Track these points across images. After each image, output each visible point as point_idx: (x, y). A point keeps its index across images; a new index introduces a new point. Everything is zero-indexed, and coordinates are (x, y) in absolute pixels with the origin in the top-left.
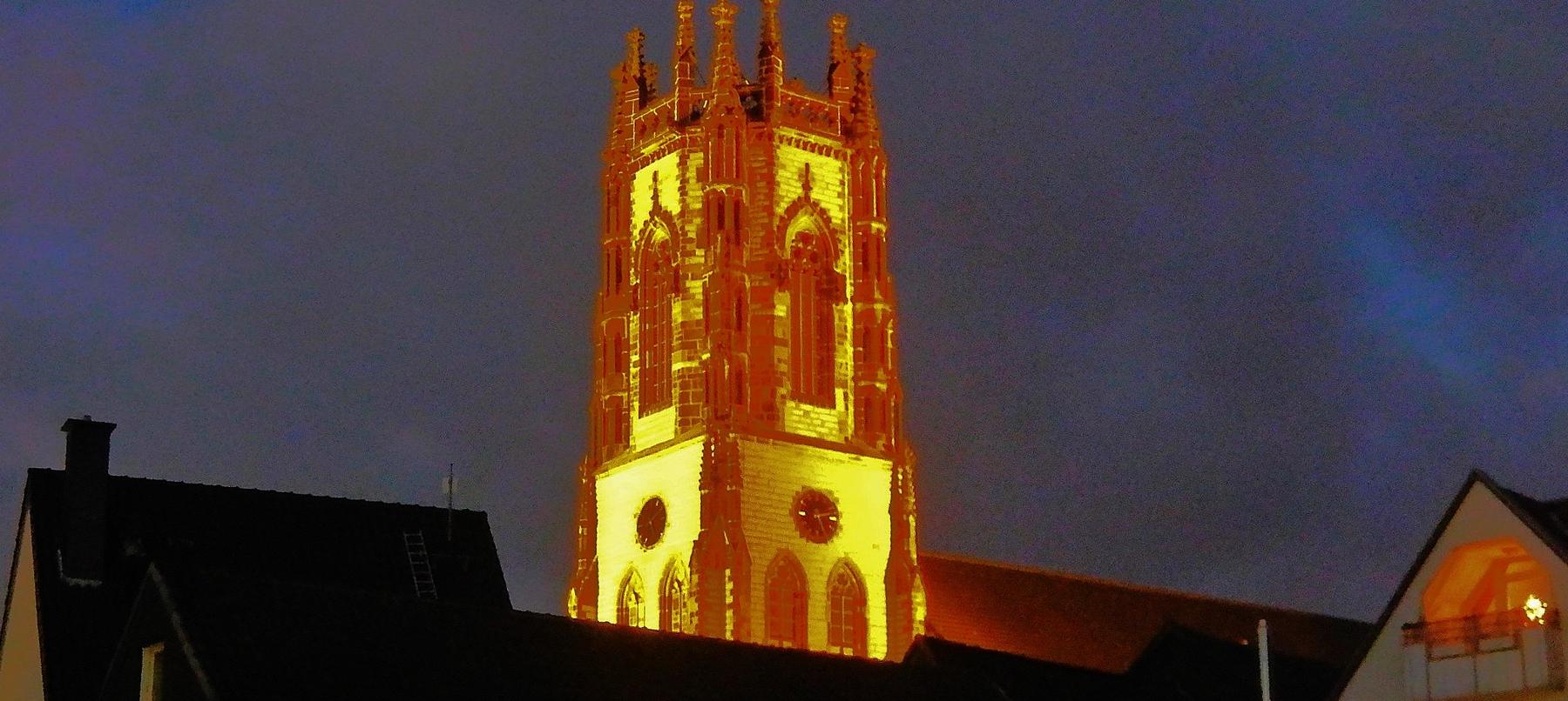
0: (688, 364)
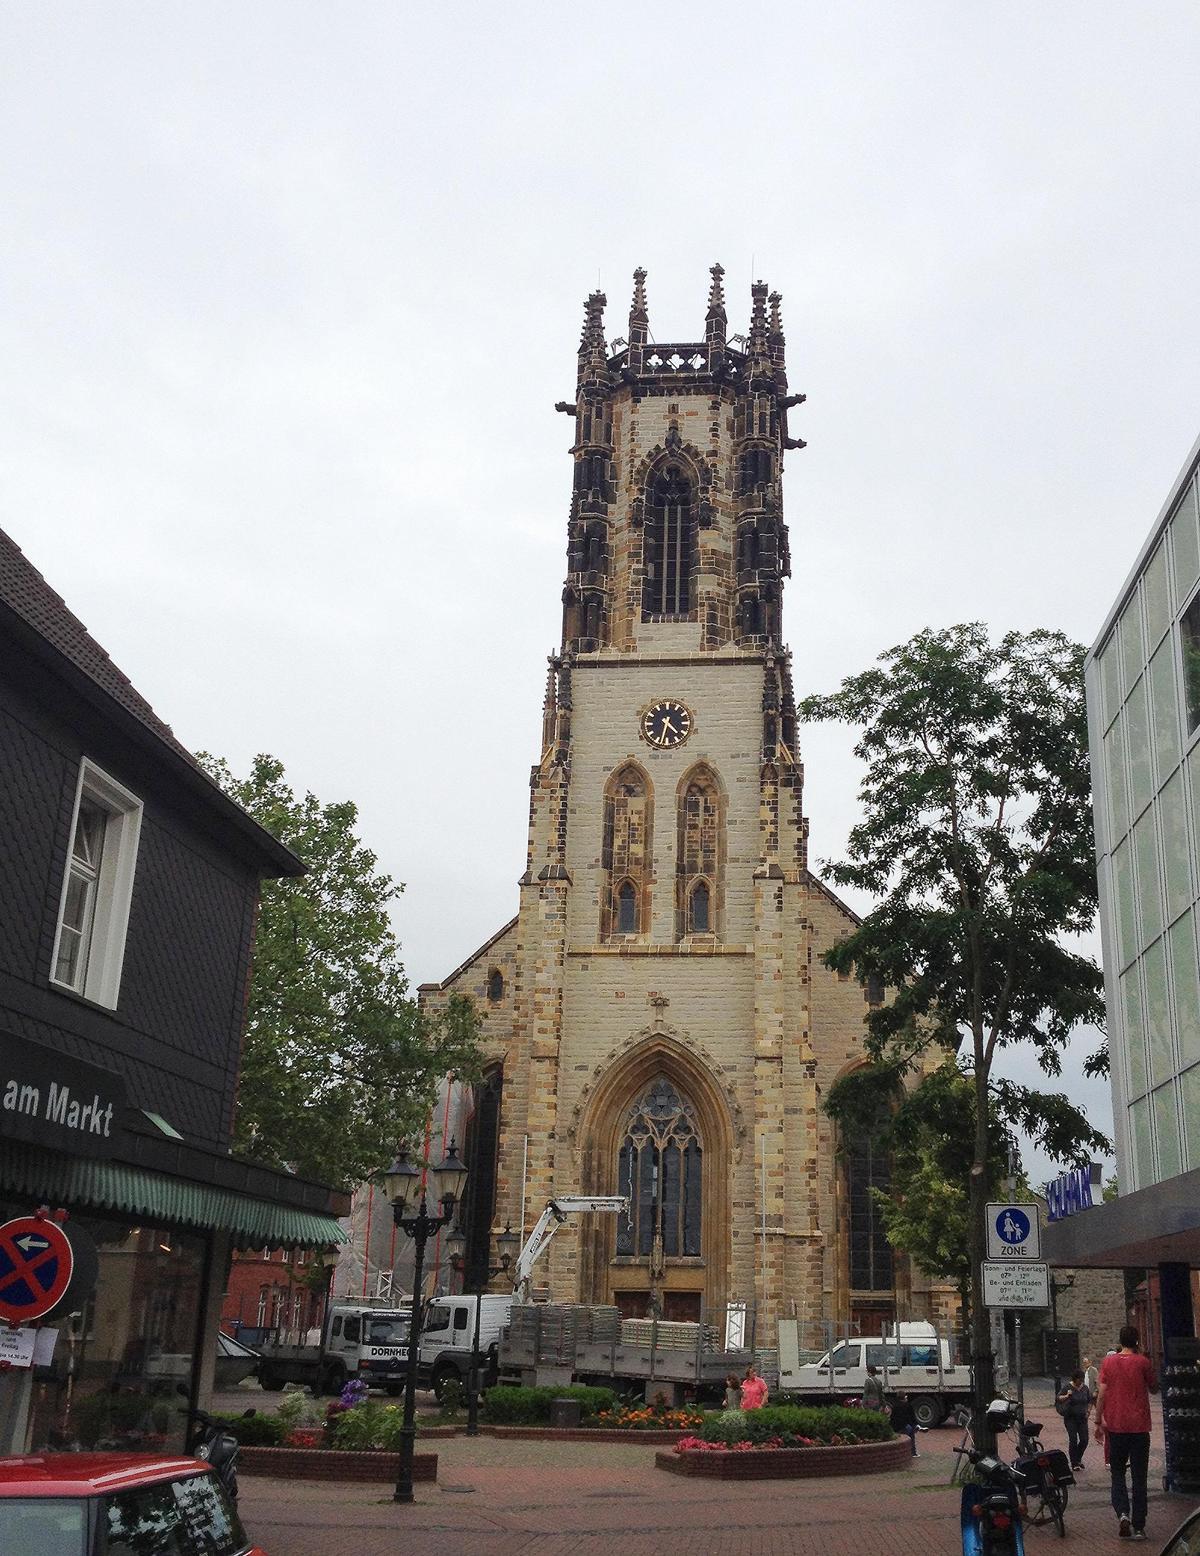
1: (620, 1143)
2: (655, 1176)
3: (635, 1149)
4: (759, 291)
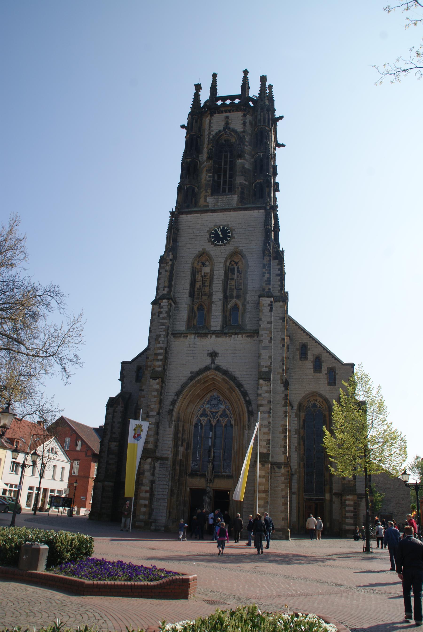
0: (245, 182)
1: (195, 421)
2: (211, 436)
3: (201, 424)
4: (263, 79)
